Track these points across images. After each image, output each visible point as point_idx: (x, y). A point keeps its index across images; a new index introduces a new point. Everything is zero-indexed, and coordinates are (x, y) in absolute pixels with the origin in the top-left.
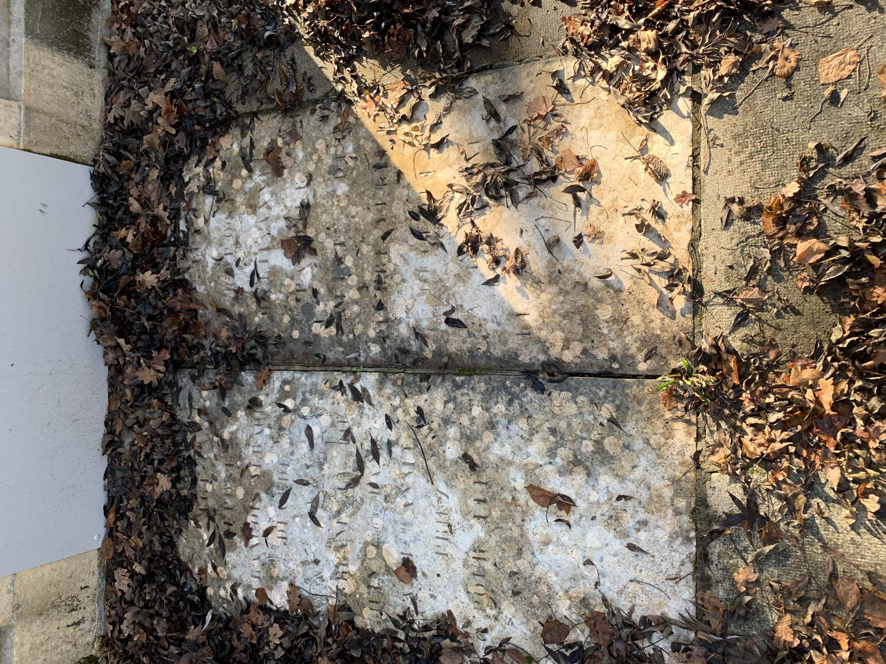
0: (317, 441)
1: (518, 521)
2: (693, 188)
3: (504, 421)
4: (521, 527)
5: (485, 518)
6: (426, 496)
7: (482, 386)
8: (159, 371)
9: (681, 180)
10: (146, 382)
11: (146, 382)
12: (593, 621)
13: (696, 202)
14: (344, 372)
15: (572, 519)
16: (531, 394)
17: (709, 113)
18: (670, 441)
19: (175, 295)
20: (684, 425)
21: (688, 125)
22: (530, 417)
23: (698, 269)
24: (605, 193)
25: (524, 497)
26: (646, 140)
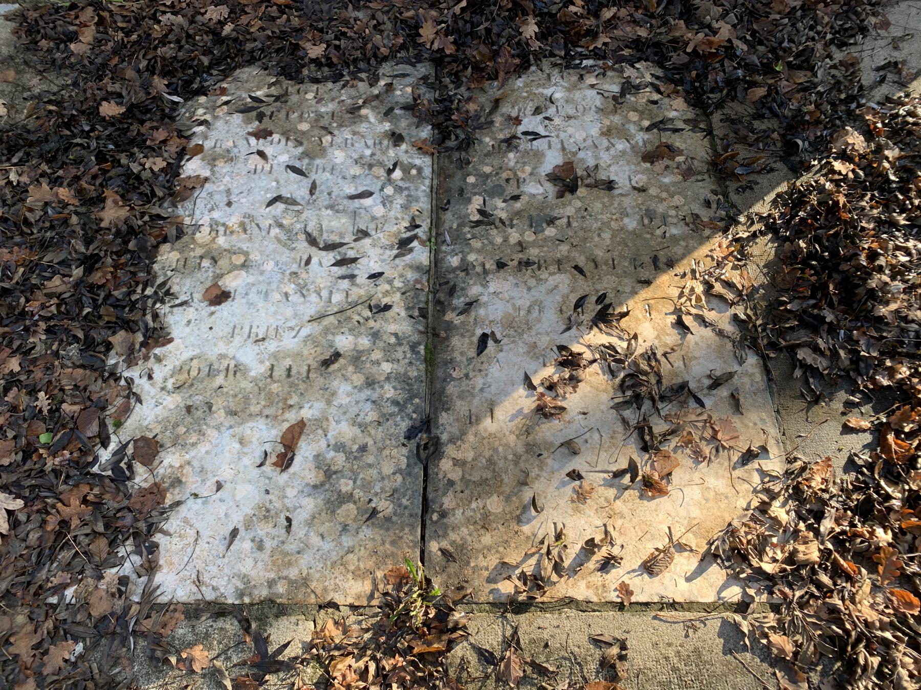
0: (357, 203)
1: (267, 412)
2: (637, 603)
3: (375, 396)
4: (260, 414)
5: (271, 376)
6: (296, 315)
7: (413, 373)
8: (432, 43)
9: (646, 589)
10: (421, 31)
11: (421, 31)
12: (156, 491)
13: (621, 607)
14: (430, 229)
15: (267, 468)
16: (404, 425)
17: (725, 622)
18: (350, 576)
19: (513, 56)
20: (368, 592)
21: (709, 597)
22: (379, 423)
23: (544, 608)
24: (630, 505)
25: (292, 417)
26: (692, 551)
